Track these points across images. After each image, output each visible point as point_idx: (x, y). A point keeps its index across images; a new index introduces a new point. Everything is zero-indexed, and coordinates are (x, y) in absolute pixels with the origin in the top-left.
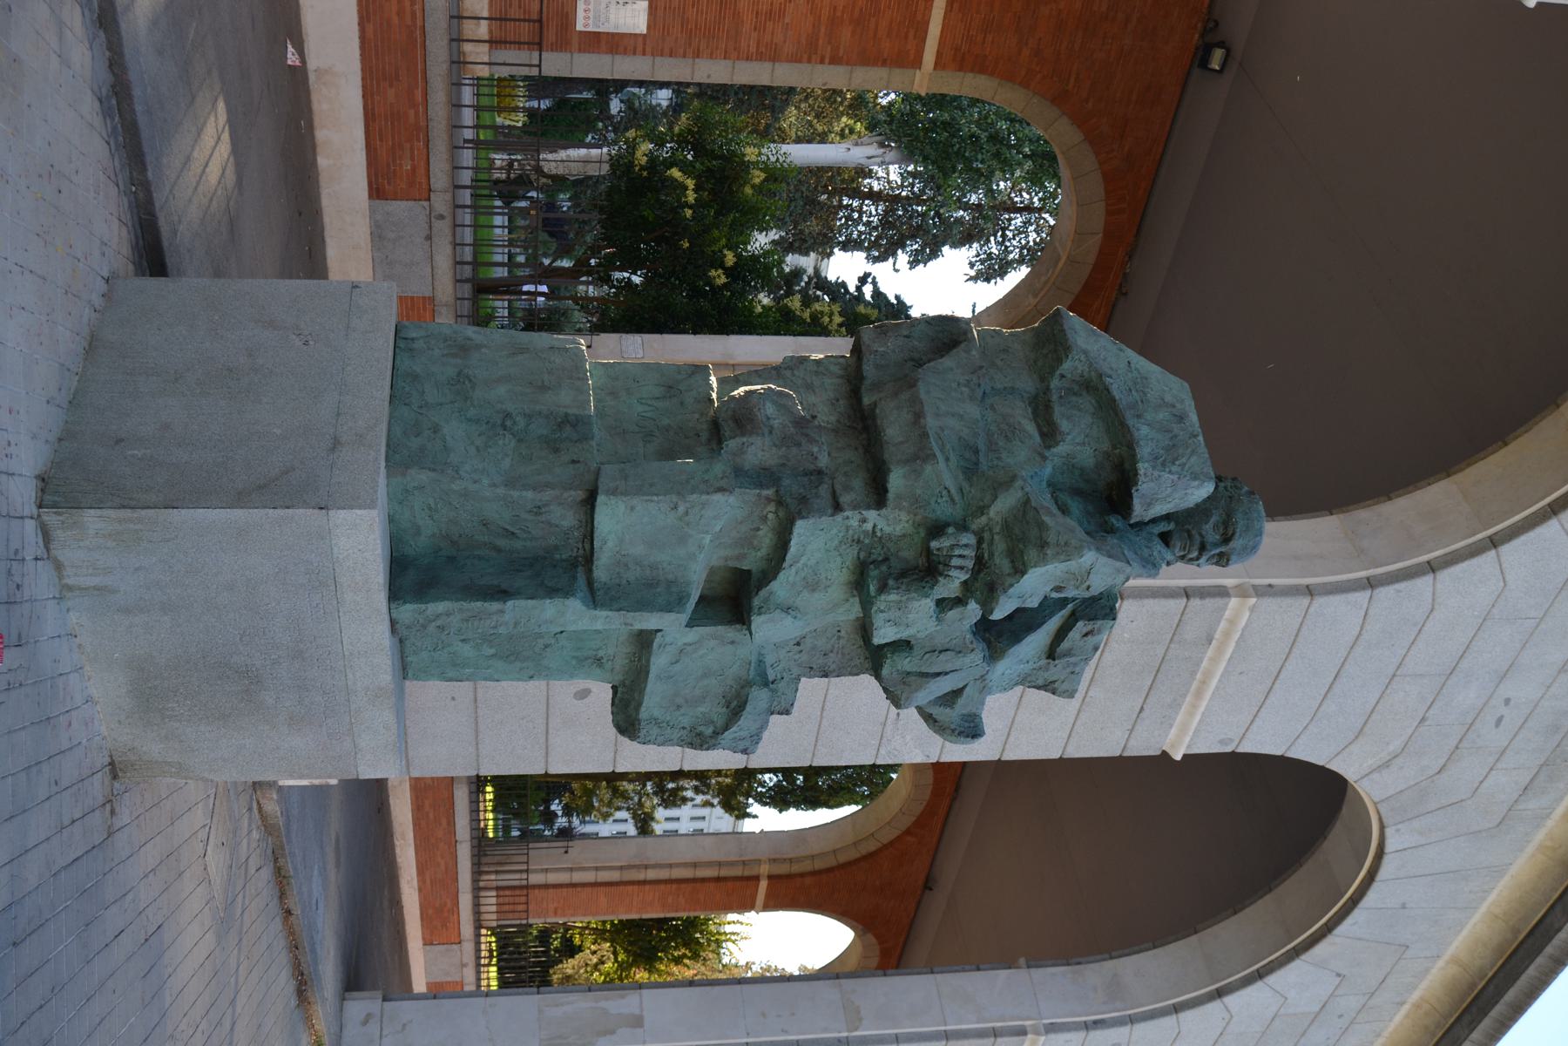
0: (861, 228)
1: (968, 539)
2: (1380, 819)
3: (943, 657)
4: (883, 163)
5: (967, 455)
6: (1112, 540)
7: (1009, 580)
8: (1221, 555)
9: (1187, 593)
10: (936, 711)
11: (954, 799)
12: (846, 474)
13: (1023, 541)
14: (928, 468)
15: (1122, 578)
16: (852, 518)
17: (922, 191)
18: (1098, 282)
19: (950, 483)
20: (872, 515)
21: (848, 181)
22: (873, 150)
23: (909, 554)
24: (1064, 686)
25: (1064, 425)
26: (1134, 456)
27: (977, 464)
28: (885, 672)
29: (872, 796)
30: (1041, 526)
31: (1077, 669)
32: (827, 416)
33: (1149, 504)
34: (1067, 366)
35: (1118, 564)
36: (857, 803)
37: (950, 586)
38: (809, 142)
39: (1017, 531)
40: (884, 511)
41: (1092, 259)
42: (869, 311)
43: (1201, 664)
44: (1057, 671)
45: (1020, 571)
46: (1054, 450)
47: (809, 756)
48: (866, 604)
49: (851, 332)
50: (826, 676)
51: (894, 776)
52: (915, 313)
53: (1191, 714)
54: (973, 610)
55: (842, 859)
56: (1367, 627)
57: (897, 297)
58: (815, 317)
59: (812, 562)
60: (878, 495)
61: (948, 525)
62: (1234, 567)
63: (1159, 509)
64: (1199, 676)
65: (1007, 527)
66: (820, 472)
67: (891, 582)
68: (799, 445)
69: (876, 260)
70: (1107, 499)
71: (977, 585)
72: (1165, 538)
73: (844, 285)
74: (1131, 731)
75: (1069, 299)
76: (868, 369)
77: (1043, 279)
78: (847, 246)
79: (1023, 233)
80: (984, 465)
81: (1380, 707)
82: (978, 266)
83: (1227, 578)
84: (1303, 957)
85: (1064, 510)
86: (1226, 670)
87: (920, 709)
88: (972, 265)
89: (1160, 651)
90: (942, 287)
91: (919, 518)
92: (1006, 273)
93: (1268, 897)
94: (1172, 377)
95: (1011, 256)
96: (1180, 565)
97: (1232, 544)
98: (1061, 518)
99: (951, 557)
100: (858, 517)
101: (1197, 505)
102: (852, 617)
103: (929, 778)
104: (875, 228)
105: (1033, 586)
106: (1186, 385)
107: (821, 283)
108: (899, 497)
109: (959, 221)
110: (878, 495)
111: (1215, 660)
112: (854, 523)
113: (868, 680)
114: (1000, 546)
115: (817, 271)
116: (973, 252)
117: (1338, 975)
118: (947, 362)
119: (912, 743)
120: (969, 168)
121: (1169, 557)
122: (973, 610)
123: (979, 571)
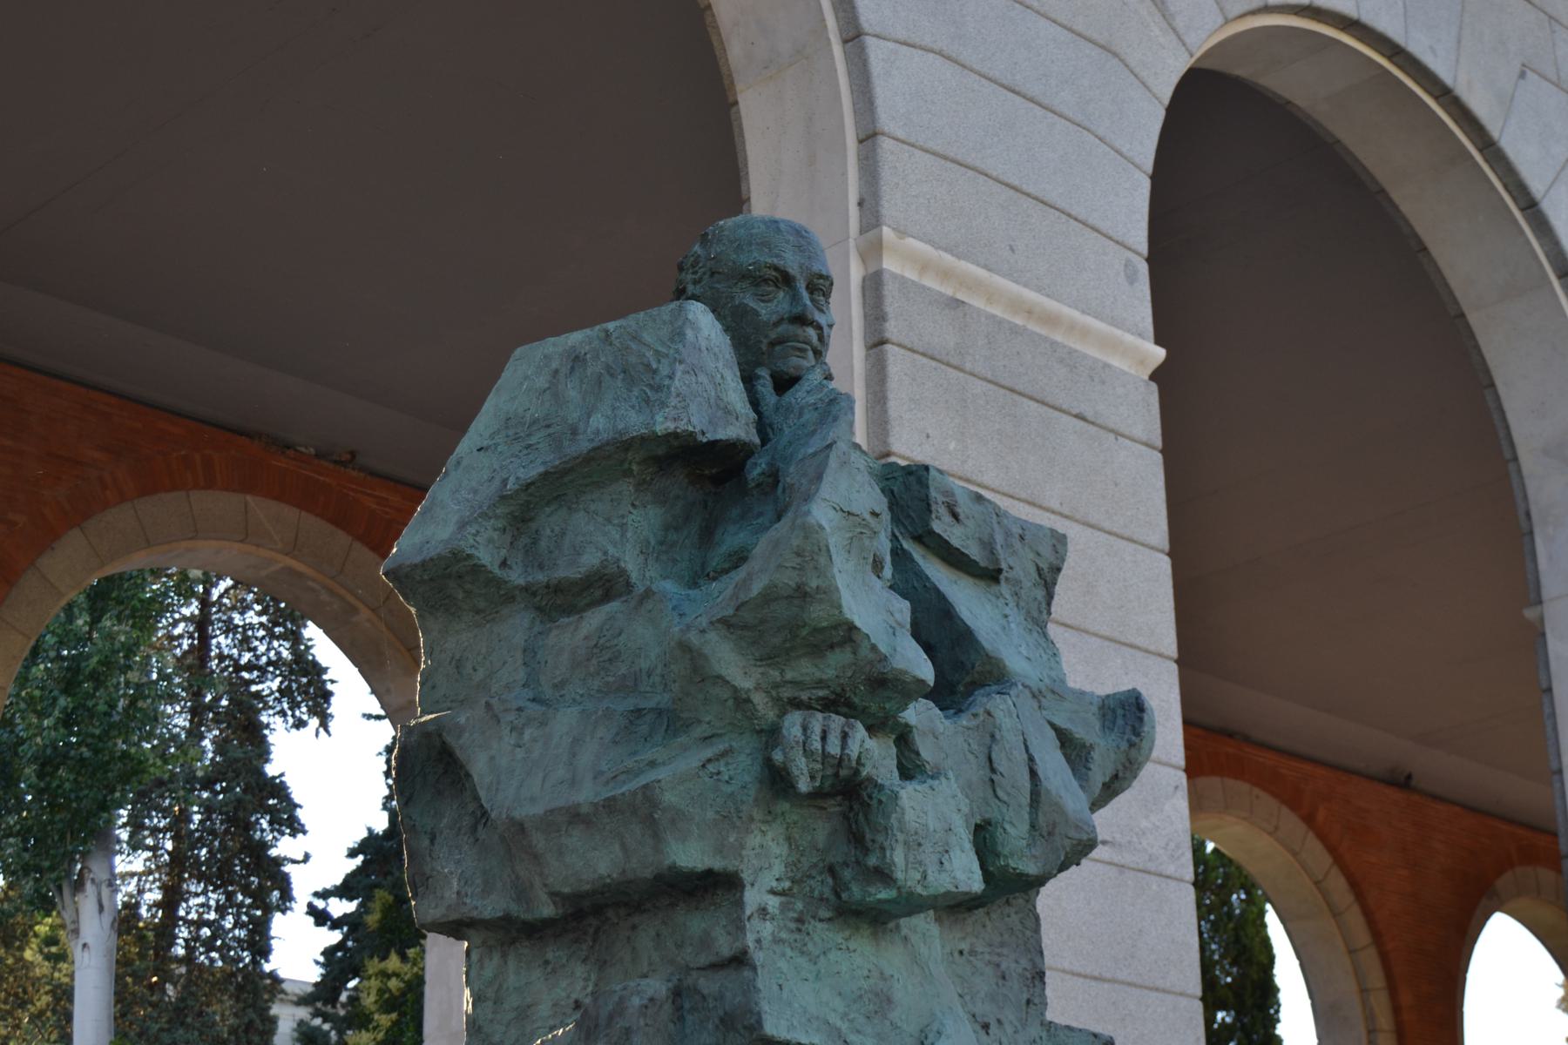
0: (228, 923)
1: (793, 725)
2: (1253, 13)
3: (1002, 764)
4: (111, 884)
5: (644, 729)
6: (791, 475)
7: (864, 651)
8: (812, 289)
9: (876, 343)
10: (1099, 776)
11: (1247, 739)
12: (679, 946)
13: (795, 627)
14: (669, 797)
15: (855, 456)
16: (758, 932)
17: (166, 812)
18: (336, 505)
19: (693, 760)
20: (753, 897)
21: (141, 945)
22: (87, 903)
23: (821, 829)
24: (1046, 551)
25: (590, 560)
26: (643, 439)
27: (659, 712)
28: (1031, 868)
29: (1249, 887)
30: (768, 597)
31: (1016, 530)
32: (576, 982)
33: (727, 411)
34: (487, 557)
35: (833, 462)
36: (1262, 913)
37: (875, 755)
38: (69, 1017)
39: (777, 640)
40: (746, 876)
41: (290, 513)
42: (377, 906)
43: (997, 316)
44: (1019, 565)
45: (848, 634)
46: (634, 576)
47: (1184, 1002)
48: (912, 904)
49: (416, 938)
50: (1040, 975)
51: (1210, 846)
52: (381, 823)
53: (1085, 333)
54: (920, 714)
55: (1363, 937)
56: (927, 41)
57: (352, 854)
58: (389, 1003)
59: (838, 1004)
60: (717, 886)
61: (768, 762)
62: (834, 272)
63: (735, 395)
64: (1019, 321)
65: (770, 658)
66: (677, 993)
67: (872, 861)
68: (628, 1032)
69: (287, 895)
70: (719, 484)
71: (874, 708)
72: (784, 383)
73: (329, 953)
74: (1118, 434)
75: (362, 553)
76: (491, 907)
77: (324, 597)
78: (260, 946)
79: (245, 633)
80: (660, 699)
81: (1061, 18)
82: (303, 712)
83: (850, 276)
84: (1495, 134)
85: (739, 558)
86: (1008, 275)
87: (1096, 805)
88: (299, 724)
89: (979, 387)
90: (336, 774)
91: (757, 814)
92: (315, 664)
93: (1396, 197)
94: (506, 374)
95: (285, 654)
96: (830, 357)
97: (793, 270)
98: (754, 564)
99: (825, 755)
100: (755, 922)
101: (727, 329)
102: (935, 929)
103: (1212, 782)
104: (230, 896)
105: (873, 611)
106: (518, 351)
107: (326, 991)
108: (720, 850)
109: (221, 746)
110: (717, 886)
111: (991, 295)
112: (767, 929)
113: (1047, 899)
114: (804, 669)
115: (303, 1001)
116: (277, 722)
117: (1522, 75)
118: (479, 767)
119: (1155, 818)
120: (124, 729)
121: (816, 377)
122: (920, 714)
123: (849, 704)
